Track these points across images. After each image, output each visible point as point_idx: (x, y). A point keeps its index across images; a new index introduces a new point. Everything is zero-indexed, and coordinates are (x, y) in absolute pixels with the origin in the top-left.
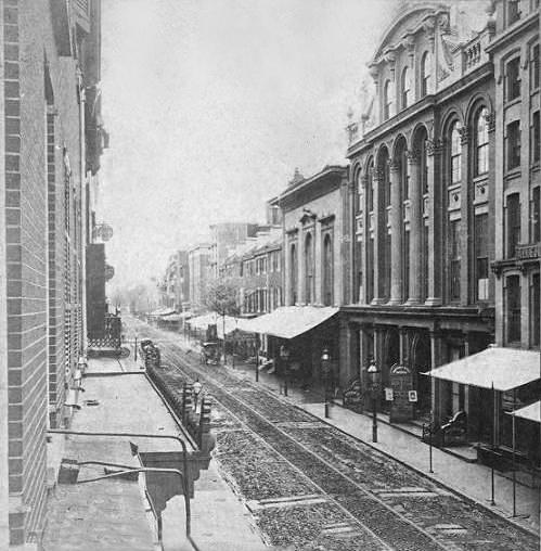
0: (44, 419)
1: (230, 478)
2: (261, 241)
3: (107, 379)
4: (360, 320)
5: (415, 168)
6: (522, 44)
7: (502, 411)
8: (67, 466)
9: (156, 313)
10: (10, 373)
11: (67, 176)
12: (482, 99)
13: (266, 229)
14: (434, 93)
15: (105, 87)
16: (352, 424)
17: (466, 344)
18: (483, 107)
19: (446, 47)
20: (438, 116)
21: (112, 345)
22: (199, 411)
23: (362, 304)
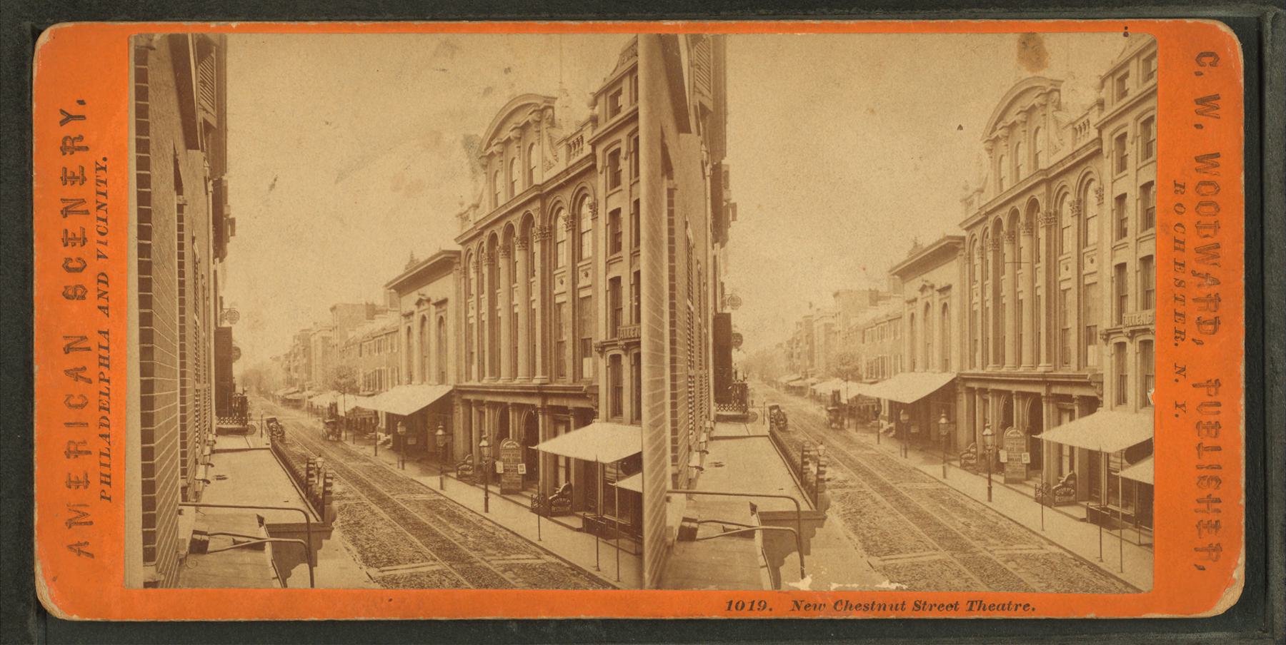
0: (176, 493)
1: (351, 547)
2: (380, 323)
4: (975, 385)
6: (1129, 118)
7: (605, 481)
9: (281, 393)
11: (196, 263)
12: (583, 188)
13: (382, 312)
15: (233, 181)
16: (467, 496)
17: (1076, 408)
18: (586, 195)
19: (551, 139)
20: (1049, 190)
21: (740, 409)
22: (321, 484)
23: (474, 382)
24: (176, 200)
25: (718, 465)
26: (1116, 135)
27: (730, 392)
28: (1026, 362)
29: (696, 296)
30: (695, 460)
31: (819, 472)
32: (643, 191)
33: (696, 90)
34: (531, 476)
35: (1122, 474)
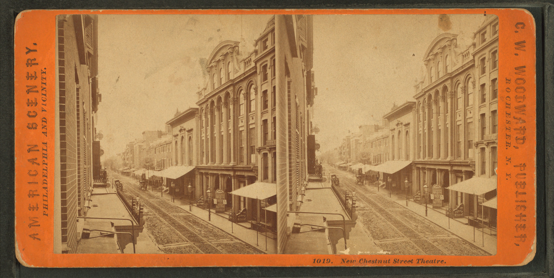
0: (76, 212)
1: (151, 236)
2: (164, 139)
3: (314, 190)
4: (420, 166)
5: (225, 109)
6: (487, 51)
7: (261, 207)
8: (296, 226)
10: (62, 194)
11: (84, 113)
12: (251, 81)
14: (233, 79)
15: (100, 78)
16: (201, 214)
17: (246, 181)
18: (252, 84)
19: (237, 60)
20: (452, 82)
22: (138, 209)
23: (204, 165)
24: (76, 86)
25: (309, 200)
26: (481, 58)
27: (314, 169)
28: (442, 156)
29: (300, 127)
30: (299, 198)
31: (353, 204)
32: (277, 82)
33: (300, 39)
34: (229, 205)
35: (484, 204)
